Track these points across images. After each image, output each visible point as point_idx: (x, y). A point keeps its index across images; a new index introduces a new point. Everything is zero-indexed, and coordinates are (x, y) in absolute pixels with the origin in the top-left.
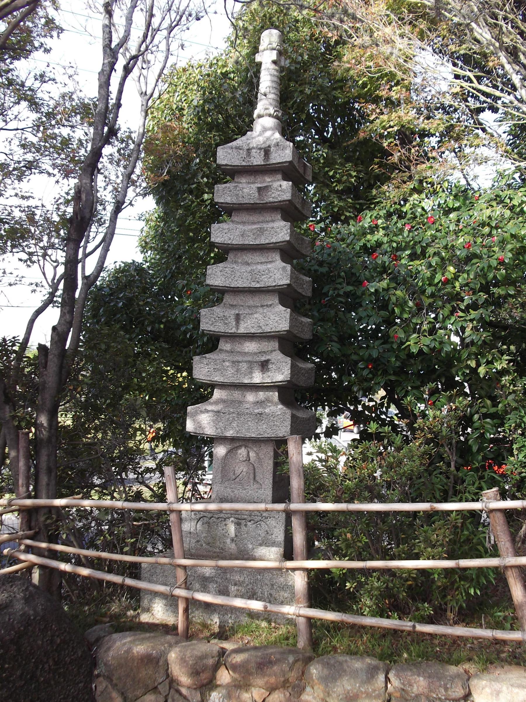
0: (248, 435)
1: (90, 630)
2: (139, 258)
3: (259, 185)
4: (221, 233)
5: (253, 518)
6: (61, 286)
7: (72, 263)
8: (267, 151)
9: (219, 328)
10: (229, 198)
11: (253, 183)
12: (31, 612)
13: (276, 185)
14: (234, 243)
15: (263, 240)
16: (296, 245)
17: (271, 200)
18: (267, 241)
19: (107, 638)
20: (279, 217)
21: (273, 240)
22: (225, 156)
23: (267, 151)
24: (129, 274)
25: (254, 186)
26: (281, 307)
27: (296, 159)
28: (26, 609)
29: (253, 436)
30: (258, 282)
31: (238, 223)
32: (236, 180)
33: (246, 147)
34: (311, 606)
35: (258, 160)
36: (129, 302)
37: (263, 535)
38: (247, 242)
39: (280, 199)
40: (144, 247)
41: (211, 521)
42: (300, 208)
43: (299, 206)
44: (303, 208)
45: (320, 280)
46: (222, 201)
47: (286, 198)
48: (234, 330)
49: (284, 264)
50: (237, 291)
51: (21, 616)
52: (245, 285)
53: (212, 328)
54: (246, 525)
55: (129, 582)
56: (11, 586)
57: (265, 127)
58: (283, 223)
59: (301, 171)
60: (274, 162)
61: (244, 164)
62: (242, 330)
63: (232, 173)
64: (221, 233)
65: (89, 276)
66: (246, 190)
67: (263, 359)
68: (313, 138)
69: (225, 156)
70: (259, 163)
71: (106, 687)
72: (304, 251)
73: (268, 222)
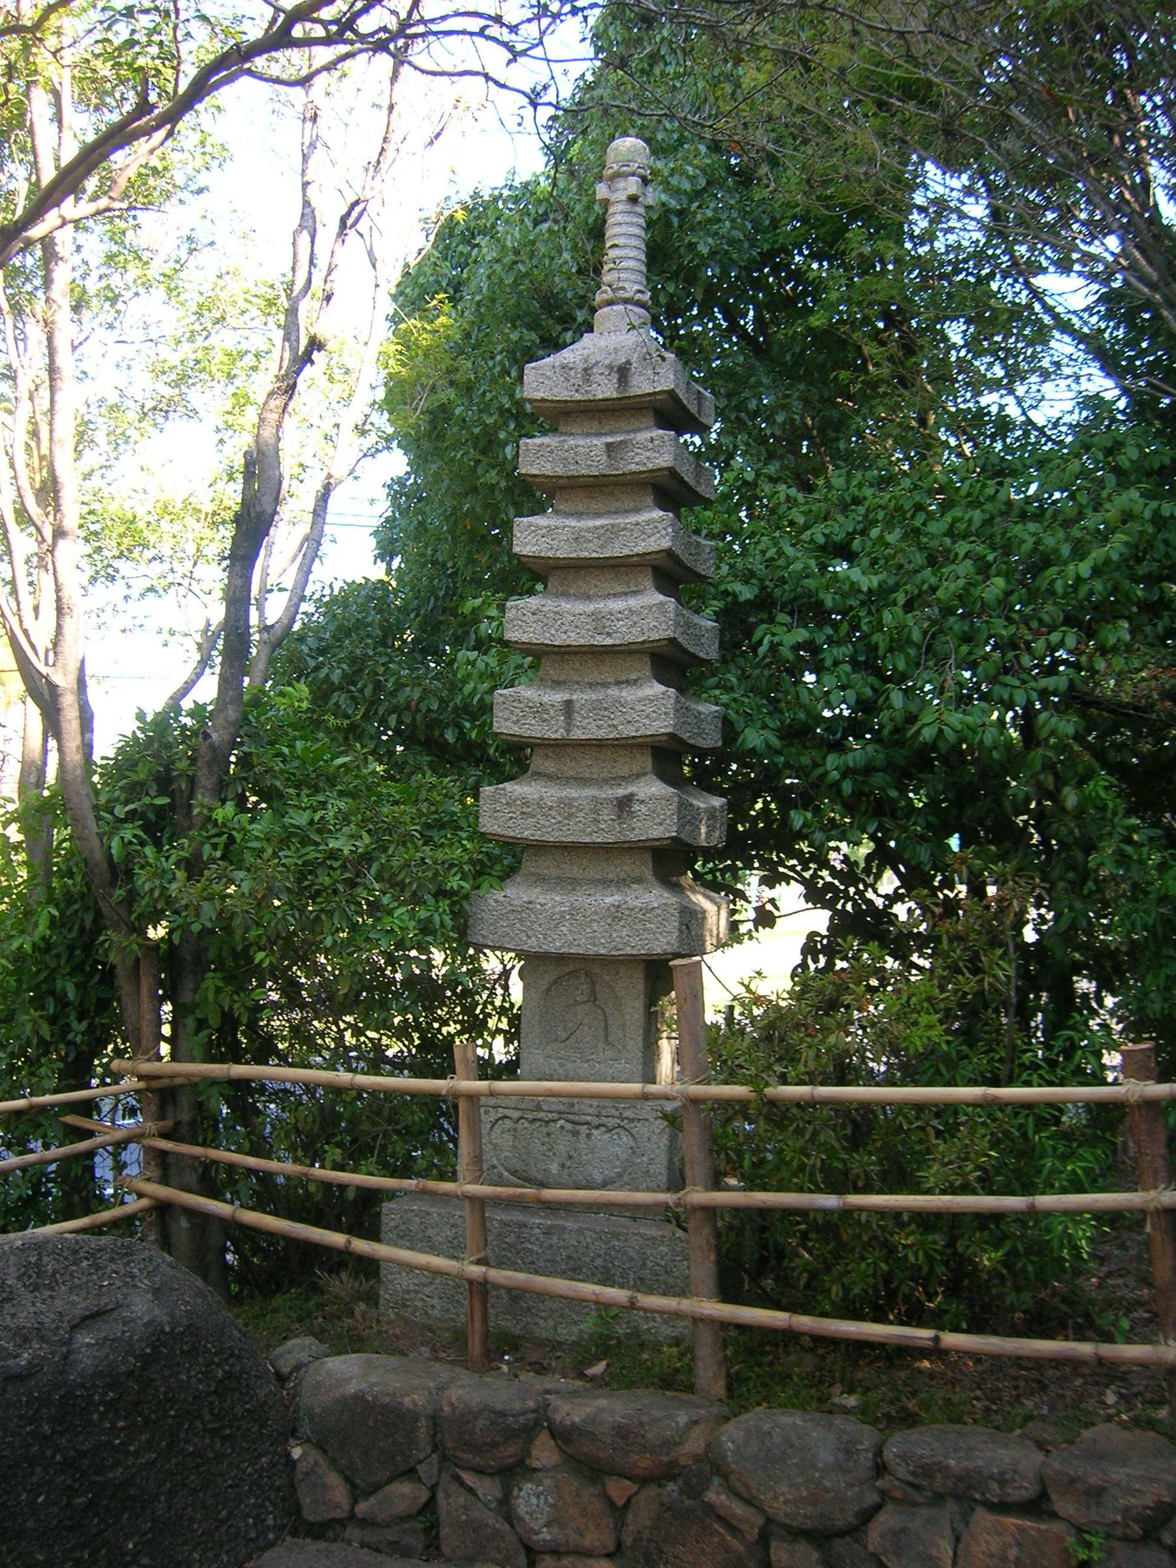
0: (593, 950)
1: (279, 1350)
2: (378, 572)
3: (609, 440)
4: (535, 535)
5: (605, 1120)
6: (220, 644)
7: (238, 599)
8: (623, 372)
9: (533, 729)
10: (549, 466)
11: (598, 435)
12: (165, 1319)
13: (642, 436)
14: (559, 554)
15: (617, 550)
16: (685, 557)
17: (633, 467)
18: (626, 552)
19: (313, 1366)
20: (650, 500)
21: (640, 549)
22: (544, 380)
23: (623, 372)
24: (356, 611)
25: (600, 442)
26: (656, 684)
27: (682, 386)
28: (157, 1312)
29: (603, 951)
30: (609, 635)
31: (568, 515)
32: (562, 429)
33: (581, 366)
34: (724, 1301)
35: (605, 389)
36: (358, 665)
37: (625, 1156)
38: (585, 554)
39: (650, 466)
40: (386, 551)
41: (519, 1126)
42: (692, 483)
43: (689, 479)
44: (698, 482)
45: (737, 622)
46: (536, 472)
47: (665, 465)
48: (560, 734)
49: (662, 598)
50: (540, 848)
51: (146, 1325)
52: (582, 642)
53: (516, 730)
54: (589, 1136)
55: (361, 1245)
56: (127, 1264)
57: (616, 343)
58: (657, 514)
59: (693, 409)
60: (640, 392)
61: (578, 397)
62: (577, 734)
63: (558, 416)
64: (535, 535)
65: (272, 626)
66: (582, 451)
67: (621, 792)
68: (717, 327)
69: (544, 380)
70: (608, 395)
71: (316, 1463)
72: (701, 570)
73: (627, 511)
